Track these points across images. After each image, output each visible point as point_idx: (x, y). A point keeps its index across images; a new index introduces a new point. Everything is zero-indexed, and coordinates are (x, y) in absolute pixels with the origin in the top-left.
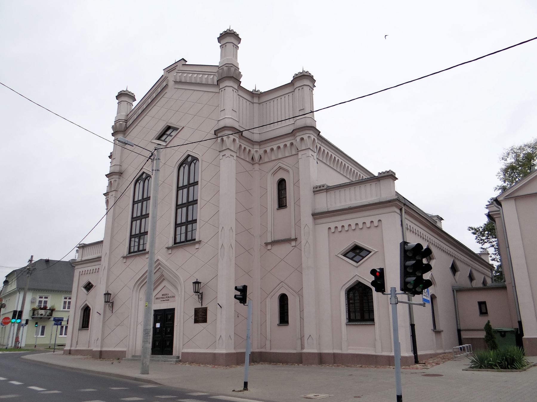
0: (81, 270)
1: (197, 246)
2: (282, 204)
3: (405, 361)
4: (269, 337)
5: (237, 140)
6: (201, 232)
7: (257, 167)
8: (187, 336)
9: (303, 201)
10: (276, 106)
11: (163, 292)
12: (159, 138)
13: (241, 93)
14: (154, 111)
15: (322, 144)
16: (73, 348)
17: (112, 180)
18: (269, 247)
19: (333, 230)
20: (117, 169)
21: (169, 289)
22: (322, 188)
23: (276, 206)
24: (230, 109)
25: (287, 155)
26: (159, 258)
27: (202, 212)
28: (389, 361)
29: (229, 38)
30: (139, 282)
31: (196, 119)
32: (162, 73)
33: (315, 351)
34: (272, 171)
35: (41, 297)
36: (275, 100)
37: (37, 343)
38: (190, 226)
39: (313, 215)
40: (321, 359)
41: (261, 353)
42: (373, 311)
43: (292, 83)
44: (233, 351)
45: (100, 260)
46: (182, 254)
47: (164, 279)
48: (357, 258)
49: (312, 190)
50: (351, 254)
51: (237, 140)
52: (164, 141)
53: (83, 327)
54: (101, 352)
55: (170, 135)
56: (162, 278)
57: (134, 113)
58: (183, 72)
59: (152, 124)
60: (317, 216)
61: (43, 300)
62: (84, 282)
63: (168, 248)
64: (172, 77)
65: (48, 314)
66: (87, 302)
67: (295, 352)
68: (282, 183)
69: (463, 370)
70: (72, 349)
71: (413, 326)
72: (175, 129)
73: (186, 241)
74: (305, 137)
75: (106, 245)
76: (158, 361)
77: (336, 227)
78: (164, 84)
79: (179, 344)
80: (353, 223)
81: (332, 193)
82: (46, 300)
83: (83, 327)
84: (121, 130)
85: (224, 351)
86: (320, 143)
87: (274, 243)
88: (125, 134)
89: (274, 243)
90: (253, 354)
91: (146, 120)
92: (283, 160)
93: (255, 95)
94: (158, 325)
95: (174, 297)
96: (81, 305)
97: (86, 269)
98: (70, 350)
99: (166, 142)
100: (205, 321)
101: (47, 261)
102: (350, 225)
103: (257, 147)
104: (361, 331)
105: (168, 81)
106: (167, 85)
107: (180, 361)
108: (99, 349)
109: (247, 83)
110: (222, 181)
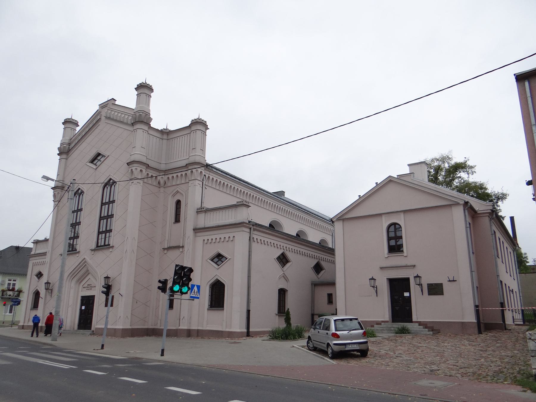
0: (34, 261)
1: (111, 250)
2: (177, 220)
3: (239, 335)
5: (144, 170)
6: (114, 239)
7: (162, 189)
8: (423, 308)
10: (181, 142)
11: (88, 283)
12: (92, 161)
13: (151, 132)
14: (89, 139)
15: (211, 174)
16: (25, 324)
17: (56, 193)
18: (166, 252)
19: (206, 241)
20: (60, 184)
21: (92, 281)
22: (202, 210)
24: (140, 146)
25: (183, 182)
26: (86, 257)
27: (116, 224)
28: (230, 335)
29: (144, 89)
31: (122, 148)
32: (97, 108)
33: (186, 328)
34: (172, 194)
36: (178, 138)
37: (6, 320)
38: (108, 234)
39: (194, 230)
40: (189, 333)
41: (154, 329)
43: (190, 126)
44: (129, 327)
46: (101, 255)
47: (89, 273)
48: (219, 263)
49: (196, 210)
51: (144, 170)
52: (95, 165)
53: (34, 307)
55: (99, 160)
56: (87, 273)
57: (76, 139)
58: (112, 110)
59: (86, 150)
60: (196, 230)
61: (12, 282)
62: (36, 271)
64: (104, 112)
65: (16, 294)
66: (37, 288)
67: (175, 328)
68: (178, 203)
70: (25, 324)
71: (248, 312)
72: (103, 156)
73: (105, 245)
76: (79, 334)
77: (216, 239)
78: (99, 117)
79: (97, 322)
80: (218, 237)
81: (208, 214)
82: (14, 282)
83: (34, 307)
84: (65, 151)
85: (121, 327)
86: (209, 173)
87: (169, 248)
88: (68, 155)
89: (169, 248)
90: (168, 330)
91: (84, 146)
92: (180, 186)
93: (166, 133)
94: (83, 308)
95: (95, 287)
96: (33, 290)
97: (38, 261)
98: (23, 326)
101: (17, 248)
102: (216, 239)
104: (216, 314)
105: (101, 115)
107: (94, 334)
109: (157, 123)
110: (131, 201)
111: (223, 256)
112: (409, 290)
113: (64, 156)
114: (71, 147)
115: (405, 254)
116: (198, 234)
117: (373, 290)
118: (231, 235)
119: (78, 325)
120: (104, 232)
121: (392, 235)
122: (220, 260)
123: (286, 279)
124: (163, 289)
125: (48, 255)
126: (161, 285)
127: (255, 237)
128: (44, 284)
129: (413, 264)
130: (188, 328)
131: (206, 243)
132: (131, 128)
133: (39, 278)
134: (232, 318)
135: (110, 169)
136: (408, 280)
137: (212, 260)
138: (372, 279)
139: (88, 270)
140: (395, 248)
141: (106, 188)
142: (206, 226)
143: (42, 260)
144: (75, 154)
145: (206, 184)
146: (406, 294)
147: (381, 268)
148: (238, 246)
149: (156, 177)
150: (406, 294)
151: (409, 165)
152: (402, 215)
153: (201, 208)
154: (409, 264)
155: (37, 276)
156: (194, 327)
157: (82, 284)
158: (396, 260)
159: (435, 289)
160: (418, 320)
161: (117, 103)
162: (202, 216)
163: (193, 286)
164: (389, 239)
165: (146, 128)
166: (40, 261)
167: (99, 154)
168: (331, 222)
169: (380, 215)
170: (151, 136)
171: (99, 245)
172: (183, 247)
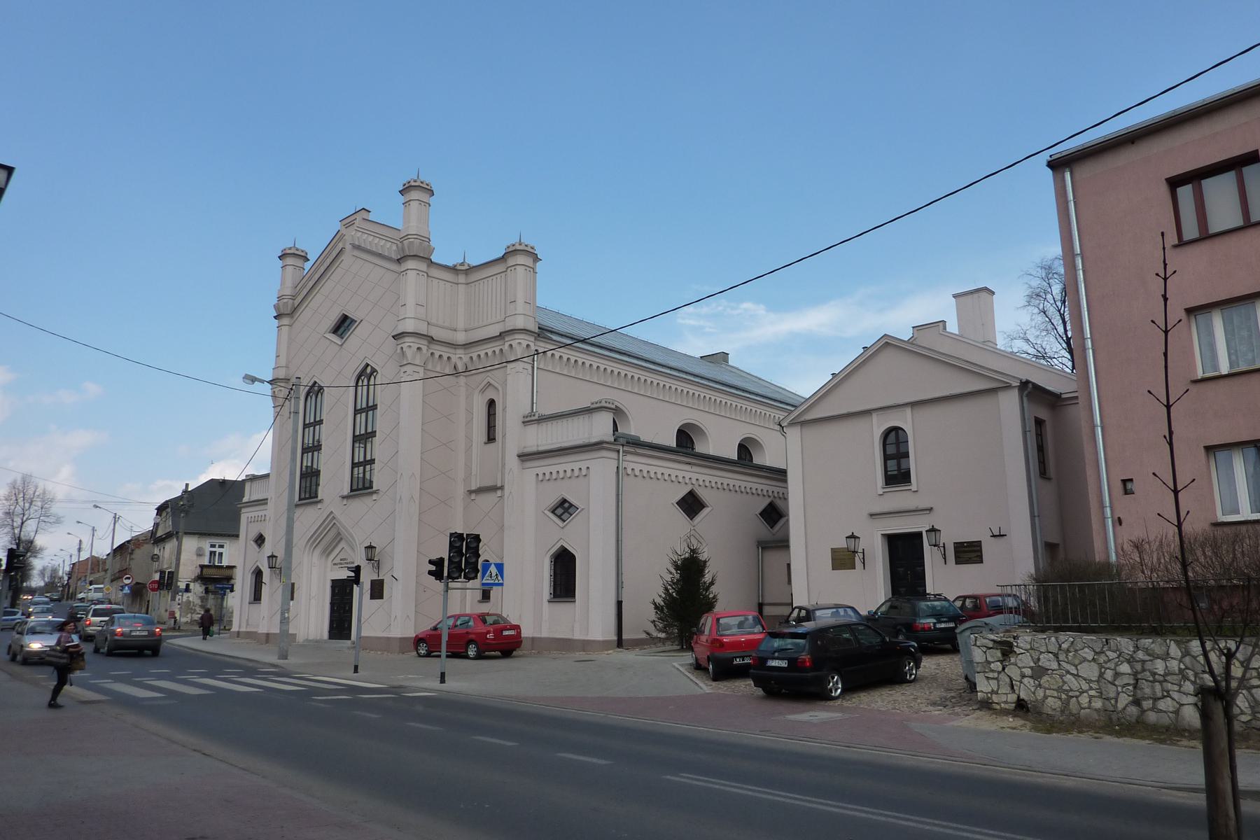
0: (250, 515)
1: (374, 497)
2: (491, 438)
5: (424, 348)
6: (379, 478)
9: (515, 436)
13: (435, 272)
18: (473, 496)
19: (541, 477)
23: (485, 438)
28: (586, 645)
35: (213, 546)
39: (519, 456)
42: (332, 604)
51: (424, 348)
54: (268, 635)
56: (339, 538)
57: (304, 286)
60: (524, 457)
62: (253, 534)
63: (343, 497)
68: (492, 403)
71: (619, 604)
74: (514, 343)
78: (340, 245)
91: (318, 299)
96: (250, 567)
100: (381, 597)
103: (460, 352)
104: (563, 608)
110: (405, 409)
111: (571, 505)
113: (286, 321)
114: (297, 302)
115: (914, 487)
116: (528, 464)
118: (583, 465)
119: (330, 632)
120: (362, 465)
121: (891, 450)
122: (566, 510)
124: (437, 574)
126: (433, 568)
127: (630, 466)
129: (928, 506)
131: (541, 480)
132: (394, 267)
133: (260, 546)
134: (591, 616)
135: (365, 345)
136: (919, 535)
139: (339, 534)
140: (897, 476)
143: (260, 513)
144: (305, 314)
147: (871, 515)
148: (596, 482)
151: (955, 296)
152: (908, 410)
153: (532, 413)
154: (921, 506)
155: (256, 541)
158: (899, 498)
159: (968, 553)
161: (371, 217)
162: (533, 429)
163: (487, 564)
164: (886, 458)
165: (423, 266)
166: (256, 514)
168: (778, 428)
169: (868, 412)
172: (502, 488)
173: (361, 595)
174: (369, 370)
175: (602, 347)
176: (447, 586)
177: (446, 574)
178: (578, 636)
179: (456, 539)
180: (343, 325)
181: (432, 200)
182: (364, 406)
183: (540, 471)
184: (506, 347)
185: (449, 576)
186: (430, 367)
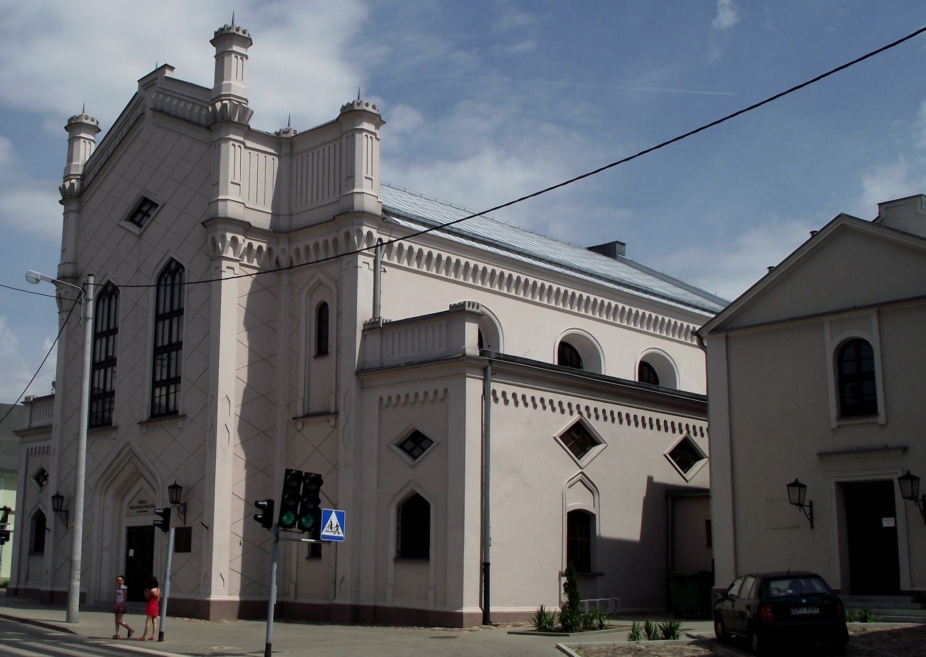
2: (322, 350)
4: (294, 579)
16: (21, 586)
19: (385, 402)
20: (69, 270)
23: (313, 352)
29: (226, 40)
30: (107, 475)
32: (135, 88)
45: (51, 432)
50: (409, 445)
51: (240, 238)
52: (139, 225)
54: (52, 593)
56: (138, 475)
67: (325, 602)
68: (323, 309)
69: (509, 633)
72: (154, 205)
75: (58, 401)
78: (139, 111)
99: (141, 226)
100: (188, 549)
104: (412, 573)
106: (143, 114)
108: (48, 588)
112: (892, 513)
113: (74, 206)
114: (86, 183)
115: (881, 419)
117: (800, 516)
123: (591, 487)
125: (56, 433)
128: (50, 500)
130: (354, 603)
136: (890, 483)
137: (401, 446)
138: (796, 484)
141: (101, 302)
142: (387, 363)
145: (385, 259)
146: (887, 522)
149: (390, 242)
150: (887, 522)
155: (37, 478)
156: (367, 600)
157: (129, 498)
158: (860, 433)
160: (915, 589)
162: (374, 339)
167: (145, 201)
170: (254, 153)
171: (157, 411)
173: (165, 544)
174: (173, 265)
175: (461, 236)
176: (277, 535)
177: (276, 520)
178: (431, 607)
179: (293, 478)
180: (142, 211)
181: (249, 51)
182: (168, 310)
183: (385, 393)
184: (341, 237)
185: (281, 523)
186: (245, 261)
